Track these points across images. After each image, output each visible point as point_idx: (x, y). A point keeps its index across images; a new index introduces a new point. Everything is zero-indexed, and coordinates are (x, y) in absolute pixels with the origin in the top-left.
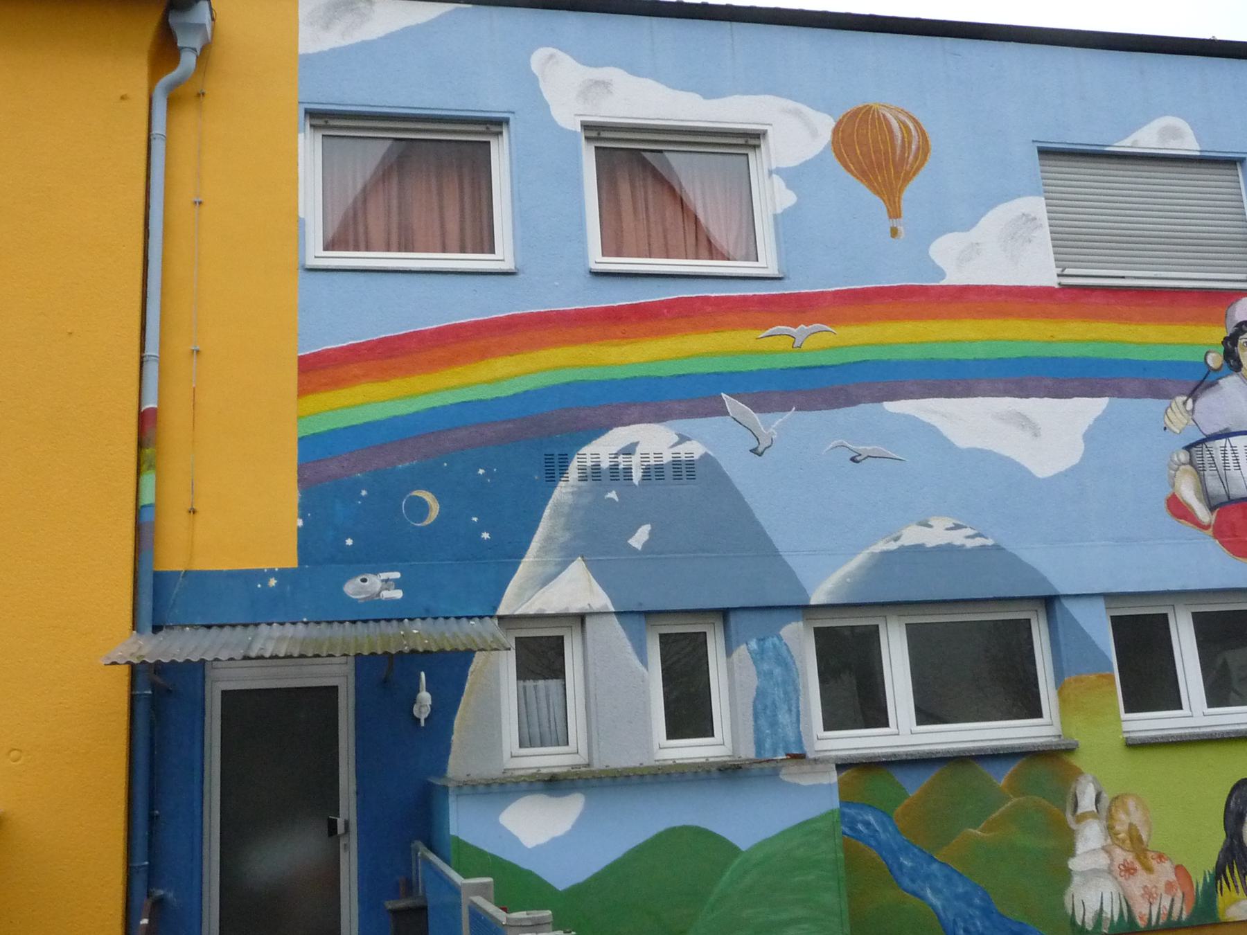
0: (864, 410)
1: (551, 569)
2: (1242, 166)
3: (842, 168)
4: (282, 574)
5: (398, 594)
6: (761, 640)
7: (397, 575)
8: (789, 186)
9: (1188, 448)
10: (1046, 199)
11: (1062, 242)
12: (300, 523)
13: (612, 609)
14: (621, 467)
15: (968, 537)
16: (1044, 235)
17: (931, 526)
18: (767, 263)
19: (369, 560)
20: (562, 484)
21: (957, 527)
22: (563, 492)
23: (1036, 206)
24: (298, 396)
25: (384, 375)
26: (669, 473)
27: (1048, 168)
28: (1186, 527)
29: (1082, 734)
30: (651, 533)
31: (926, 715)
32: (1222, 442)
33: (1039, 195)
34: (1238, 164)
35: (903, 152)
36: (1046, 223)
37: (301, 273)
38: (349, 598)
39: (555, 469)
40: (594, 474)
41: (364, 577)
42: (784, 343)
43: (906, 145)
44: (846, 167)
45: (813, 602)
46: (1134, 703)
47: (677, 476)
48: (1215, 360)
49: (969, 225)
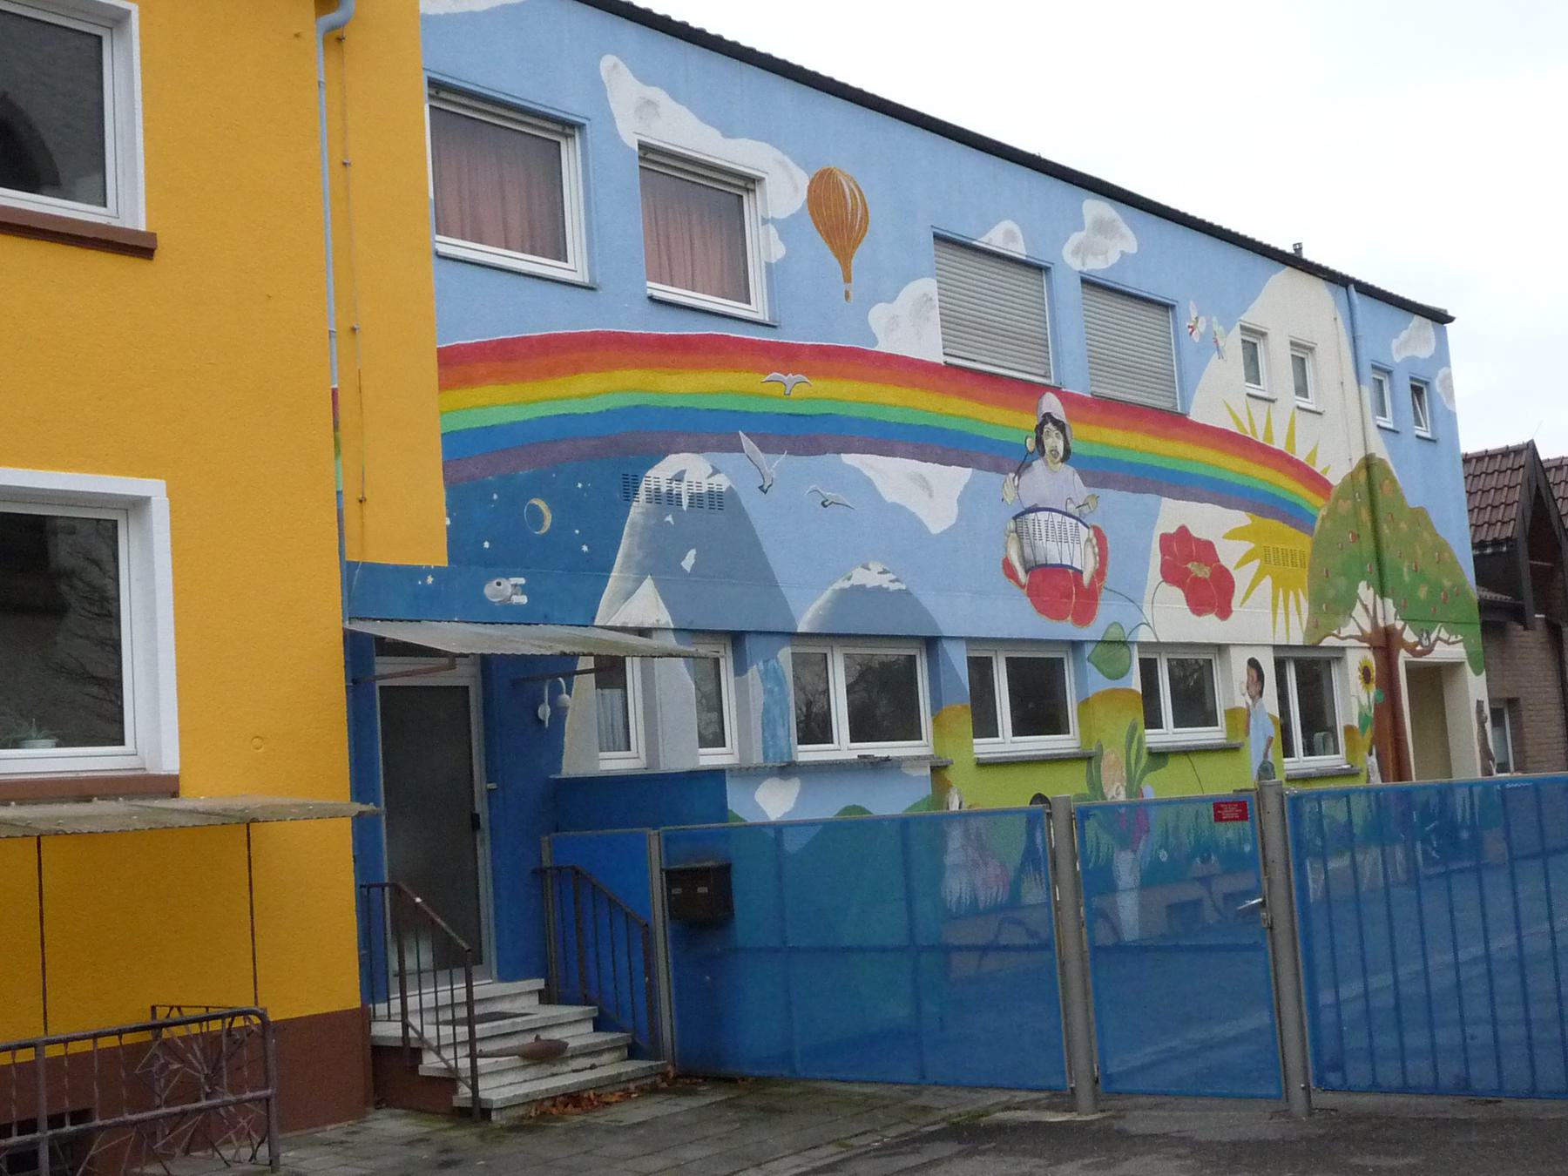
0: (829, 457)
1: (629, 585)
2: (580, 133)
3: (815, 229)
4: (437, 572)
5: (523, 599)
6: (766, 662)
7: (522, 581)
8: (782, 237)
9: (1015, 518)
10: (938, 281)
11: (949, 322)
12: (448, 522)
13: (672, 626)
14: (674, 492)
15: (891, 581)
16: (935, 315)
17: (869, 569)
18: (757, 309)
19: (500, 565)
20: (635, 504)
21: (884, 572)
22: (638, 510)
23: (927, 286)
24: (440, 389)
25: (503, 378)
26: (706, 501)
27: (941, 254)
28: (1011, 583)
29: (950, 753)
30: (697, 557)
31: (856, 736)
32: (1032, 516)
33: (933, 277)
34: (576, 130)
35: (852, 219)
36: (937, 303)
37: (436, 261)
38: (488, 600)
39: (630, 488)
40: (656, 497)
41: (498, 580)
42: (778, 390)
43: (854, 215)
44: (818, 228)
45: (799, 631)
46: (979, 733)
47: (712, 506)
48: (1031, 445)
49: (892, 300)
